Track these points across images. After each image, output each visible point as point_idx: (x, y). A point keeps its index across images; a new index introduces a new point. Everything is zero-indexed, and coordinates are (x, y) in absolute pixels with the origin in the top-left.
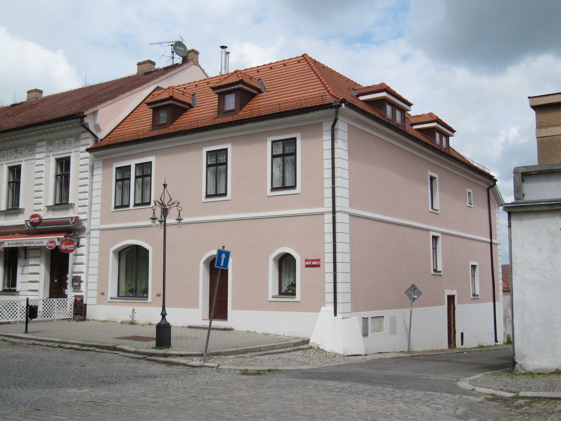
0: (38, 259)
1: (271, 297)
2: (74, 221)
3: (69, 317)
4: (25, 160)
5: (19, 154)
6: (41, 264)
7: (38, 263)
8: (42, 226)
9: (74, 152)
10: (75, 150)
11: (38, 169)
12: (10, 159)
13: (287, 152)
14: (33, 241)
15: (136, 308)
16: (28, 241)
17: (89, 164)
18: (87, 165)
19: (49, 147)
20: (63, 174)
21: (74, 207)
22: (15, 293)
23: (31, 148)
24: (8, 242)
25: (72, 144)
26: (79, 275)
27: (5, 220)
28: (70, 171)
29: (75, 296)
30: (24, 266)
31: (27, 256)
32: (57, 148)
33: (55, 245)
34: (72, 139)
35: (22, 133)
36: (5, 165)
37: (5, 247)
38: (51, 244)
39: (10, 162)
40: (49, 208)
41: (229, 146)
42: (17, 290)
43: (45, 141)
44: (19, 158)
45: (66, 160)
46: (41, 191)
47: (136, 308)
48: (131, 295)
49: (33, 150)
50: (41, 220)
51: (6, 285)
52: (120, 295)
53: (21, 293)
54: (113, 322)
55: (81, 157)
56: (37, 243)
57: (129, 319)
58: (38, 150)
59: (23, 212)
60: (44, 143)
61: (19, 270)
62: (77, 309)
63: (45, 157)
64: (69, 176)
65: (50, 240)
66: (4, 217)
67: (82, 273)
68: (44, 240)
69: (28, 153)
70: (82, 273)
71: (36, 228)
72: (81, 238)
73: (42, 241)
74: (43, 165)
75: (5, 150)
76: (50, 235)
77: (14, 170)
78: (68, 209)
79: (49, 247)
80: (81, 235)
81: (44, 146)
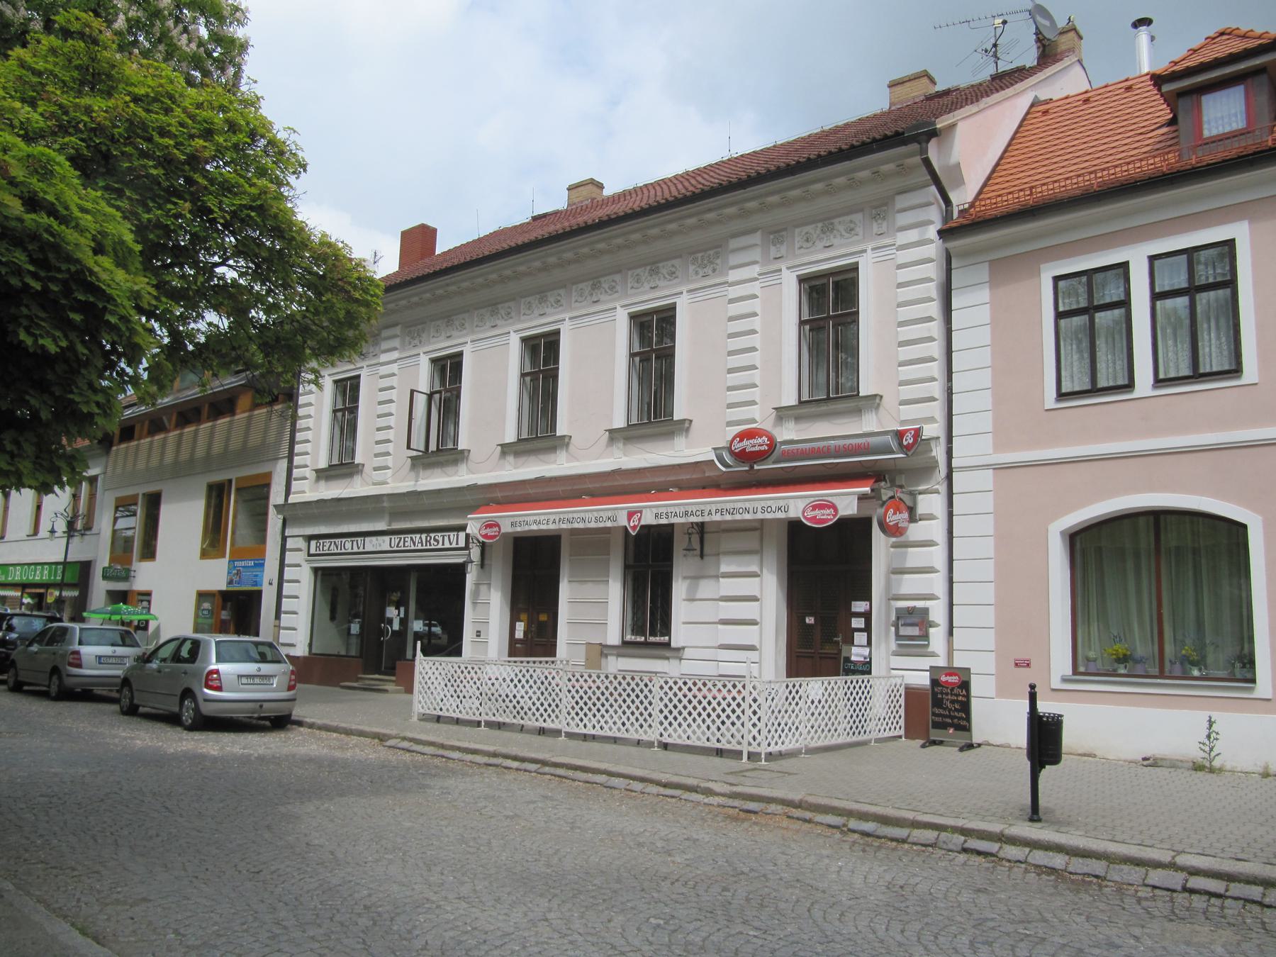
0: (756, 558)
1: (1059, 679)
2: (911, 441)
3: (896, 733)
4: (873, 249)
5: (665, 277)
6: (765, 571)
7: (754, 568)
8: (774, 462)
9: (873, 249)
10: (475, 337)
11: (735, 309)
12: (434, 343)
13: (1203, 281)
14: (747, 505)
15: (1216, 715)
16: (729, 506)
17: (934, 276)
18: (929, 280)
19: (773, 249)
20: (346, 409)
21: (879, 405)
22: (668, 654)
23: (880, 210)
24: (512, 520)
25: (859, 230)
26: (920, 604)
27: (625, 455)
28: (460, 383)
29: (931, 667)
30: (696, 578)
31: (707, 549)
32: (801, 247)
33: (835, 516)
34: (858, 217)
35: (726, 206)
36: (785, 273)
37: (643, 523)
38: (817, 512)
39: (806, 259)
40: (506, 449)
41: (1239, 231)
42: (673, 645)
43: (759, 234)
44: (459, 337)
45: (837, 279)
46: (754, 367)
47: (1216, 715)
48: (1122, 671)
49: (712, 263)
50: (772, 444)
51: (629, 630)
52: (1082, 669)
53: (688, 653)
54: (1079, 755)
55: (900, 261)
56: (597, 520)
57: (1197, 754)
58: (385, 345)
59: (688, 430)
60: (756, 238)
61: (679, 589)
62: (945, 709)
63: (760, 275)
64: (672, 356)
65: (812, 499)
66: (621, 445)
67: (931, 597)
68: (791, 501)
69: (697, 273)
70: (931, 597)
71: (756, 467)
72: (920, 493)
73: (781, 503)
74: (754, 297)
75: (619, 272)
76: (745, 491)
77: (346, 386)
78: (858, 412)
79: (813, 519)
80: (918, 485)
81: (756, 245)
